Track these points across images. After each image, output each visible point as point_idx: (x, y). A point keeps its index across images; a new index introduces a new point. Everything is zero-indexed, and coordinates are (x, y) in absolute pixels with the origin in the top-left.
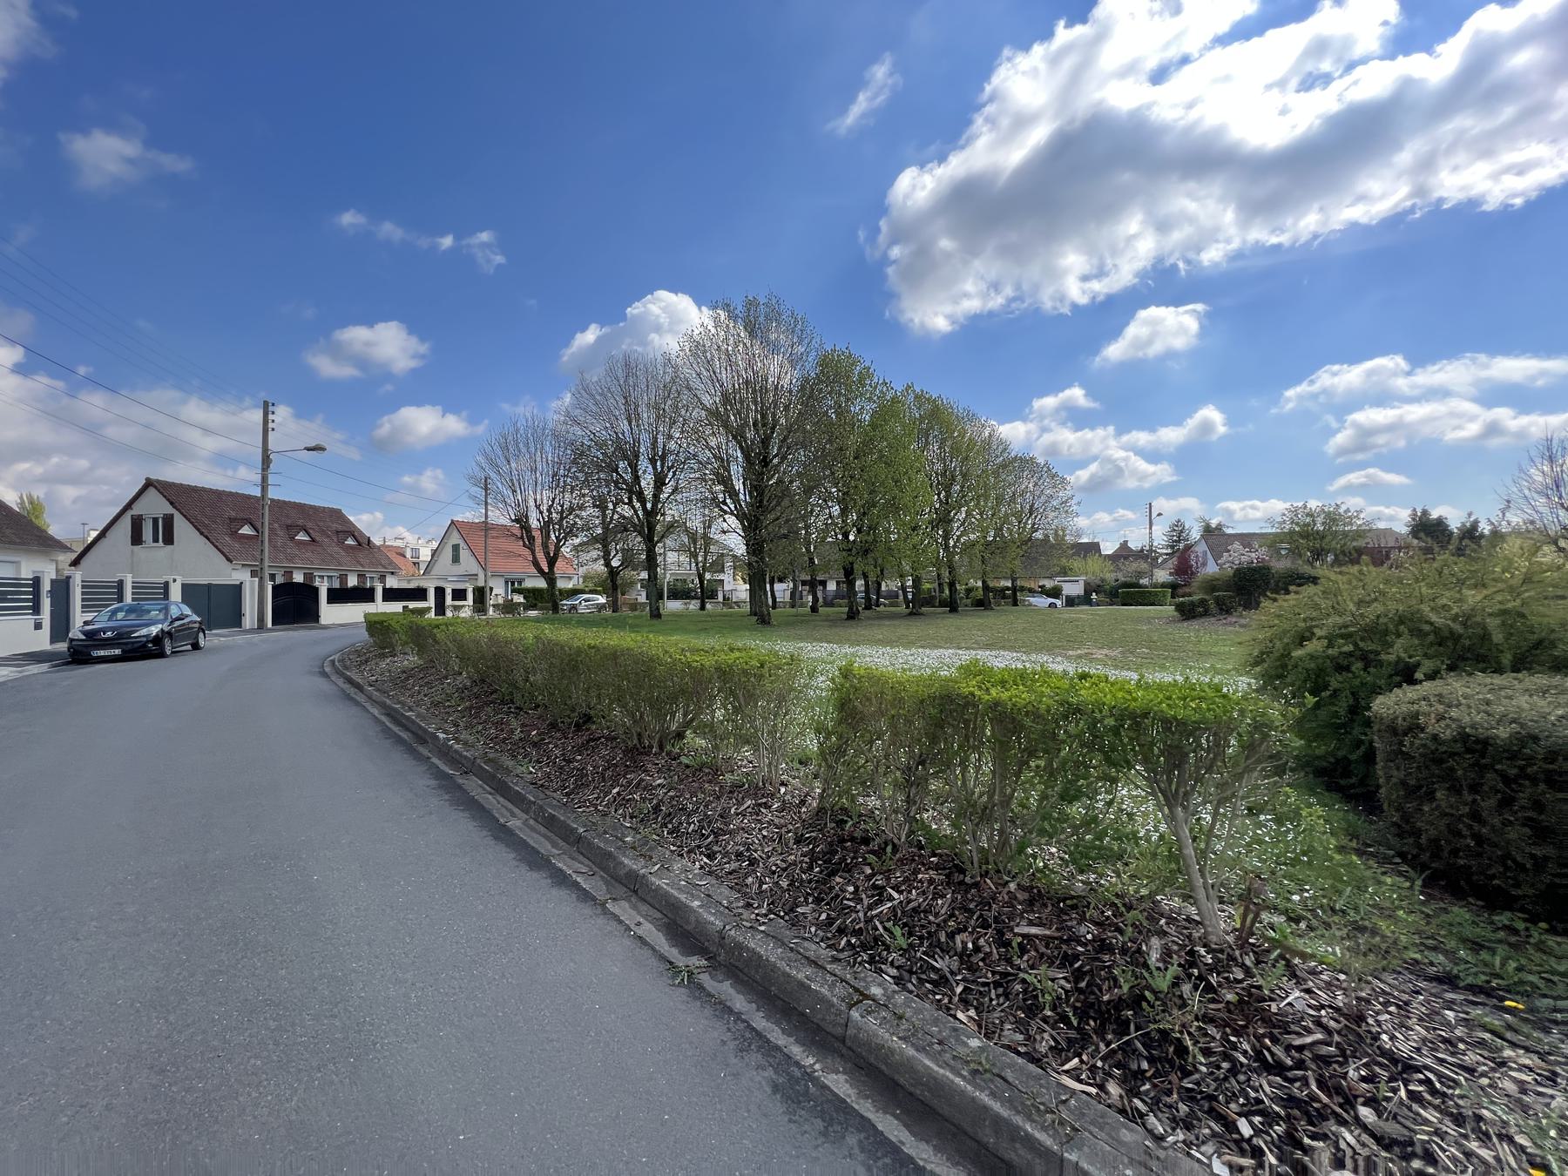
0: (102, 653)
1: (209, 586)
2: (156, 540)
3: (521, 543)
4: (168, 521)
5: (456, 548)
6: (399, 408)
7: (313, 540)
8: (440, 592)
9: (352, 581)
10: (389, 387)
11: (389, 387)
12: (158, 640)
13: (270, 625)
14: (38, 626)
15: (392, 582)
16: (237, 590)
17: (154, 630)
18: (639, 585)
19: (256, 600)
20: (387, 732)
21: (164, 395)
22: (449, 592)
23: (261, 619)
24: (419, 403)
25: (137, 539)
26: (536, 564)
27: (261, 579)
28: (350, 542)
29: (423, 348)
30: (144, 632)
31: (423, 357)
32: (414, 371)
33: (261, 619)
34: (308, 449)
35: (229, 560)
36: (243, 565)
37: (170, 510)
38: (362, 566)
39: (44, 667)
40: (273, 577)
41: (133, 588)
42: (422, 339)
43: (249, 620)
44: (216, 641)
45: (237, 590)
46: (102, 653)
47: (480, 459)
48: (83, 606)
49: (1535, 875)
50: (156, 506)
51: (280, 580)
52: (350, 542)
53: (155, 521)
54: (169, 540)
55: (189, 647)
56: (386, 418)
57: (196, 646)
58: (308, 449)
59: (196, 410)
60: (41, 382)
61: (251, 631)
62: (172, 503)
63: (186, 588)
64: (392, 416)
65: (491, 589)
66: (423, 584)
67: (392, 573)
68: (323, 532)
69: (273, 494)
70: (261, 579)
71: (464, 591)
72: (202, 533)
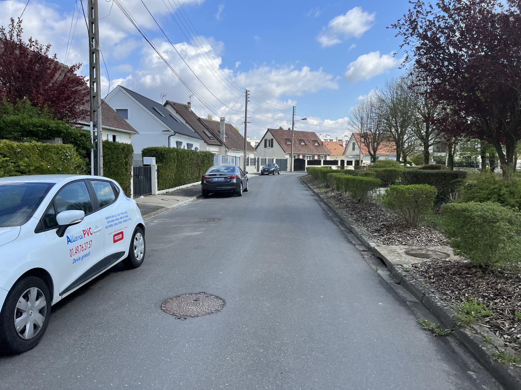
0: (266, 173)
1: (281, 159)
2: (269, 146)
3: (364, 144)
4: (272, 140)
5: (354, 144)
6: (358, 58)
7: (306, 144)
8: (342, 162)
9: (316, 158)
10: (353, 46)
11: (353, 46)
12: (273, 171)
13: (293, 171)
14: (255, 168)
15: (328, 158)
16: (286, 160)
17: (273, 169)
18: (433, 160)
19: (290, 164)
20: (327, 215)
21: (264, 69)
22: (346, 162)
23: (291, 169)
24: (367, 53)
25: (265, 146)
26: (369, 152)
27: (291, 157)
28: (316, 144)
29: (371, 18)
30: (271, 169)
31: (371, 23)
32: (366, 33)
33: (291, 169)
34: (303, 119)
35: (285, 152)
36: (288, 153)
37: (273, 138)
38: (319, 152)
39: (258, 175)
40: (295, 156)
41: (250, 160)
42: (370, 13)
43: (288, 169)
44: (282, 173)
45: (286, 160)
46: (266, 173)
47: (356, 108)
48: (250, 164)
49: (68, 95)
50: (269, 137)
51: (296, 158)
52: (316, 144)
53: (269, 140)
54: (272, 146)
55: (277, 174)
56: (351, 64)
57: (279, 174)
58: (303, 119)
59: (276, 76)
60: (227, 71)
61: (289, 172)
62: (273, 136)
63: (276, 160)
64: (355, 62)
65: (362, 161)
66: (337, 159)
67: (329, 155)
68: (309, 141)
69: (295, 129)
70: (291, 157)
71: (352, 161)
72: (279, 144)
